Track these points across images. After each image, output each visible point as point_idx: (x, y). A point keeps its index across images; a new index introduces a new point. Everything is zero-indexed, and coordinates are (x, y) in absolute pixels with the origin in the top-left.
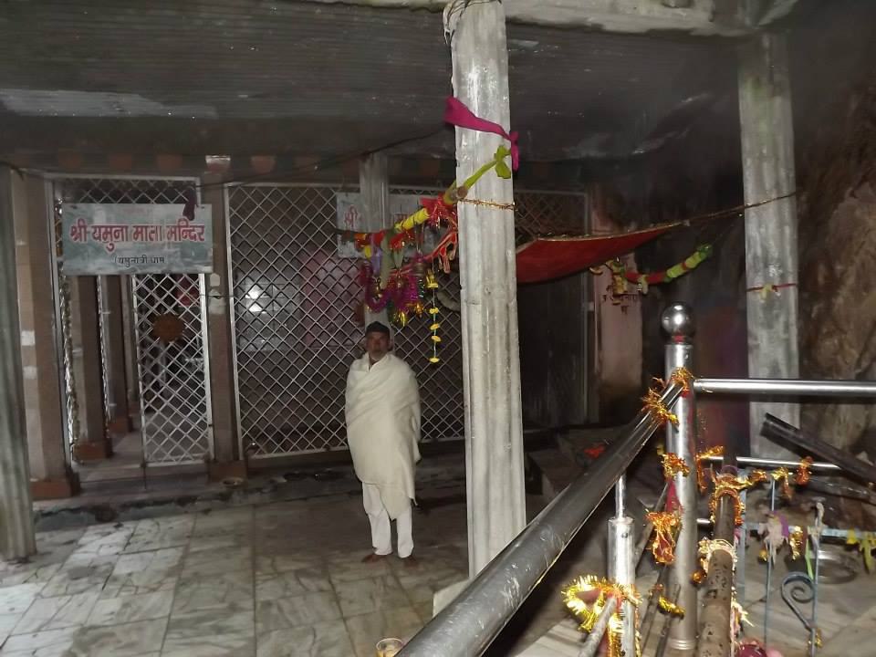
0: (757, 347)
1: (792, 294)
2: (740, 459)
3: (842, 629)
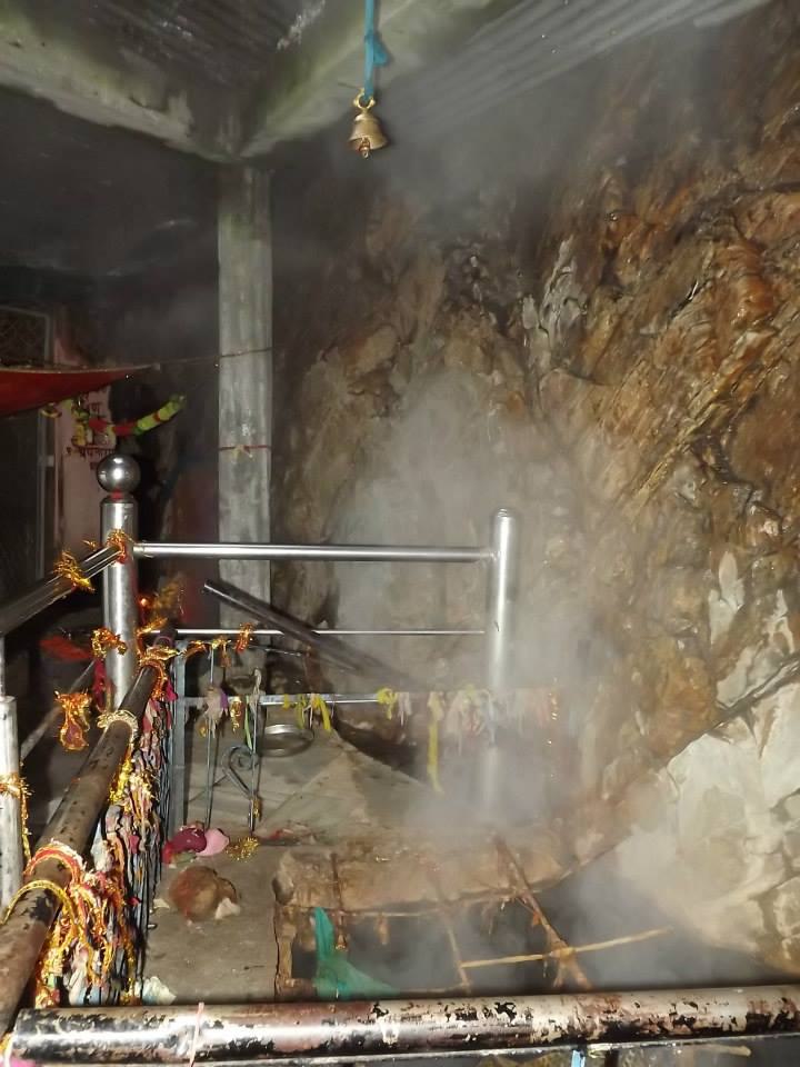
0: (228, 512)
1: (265, 458)
2: (180, 631)
3: (290, 798)
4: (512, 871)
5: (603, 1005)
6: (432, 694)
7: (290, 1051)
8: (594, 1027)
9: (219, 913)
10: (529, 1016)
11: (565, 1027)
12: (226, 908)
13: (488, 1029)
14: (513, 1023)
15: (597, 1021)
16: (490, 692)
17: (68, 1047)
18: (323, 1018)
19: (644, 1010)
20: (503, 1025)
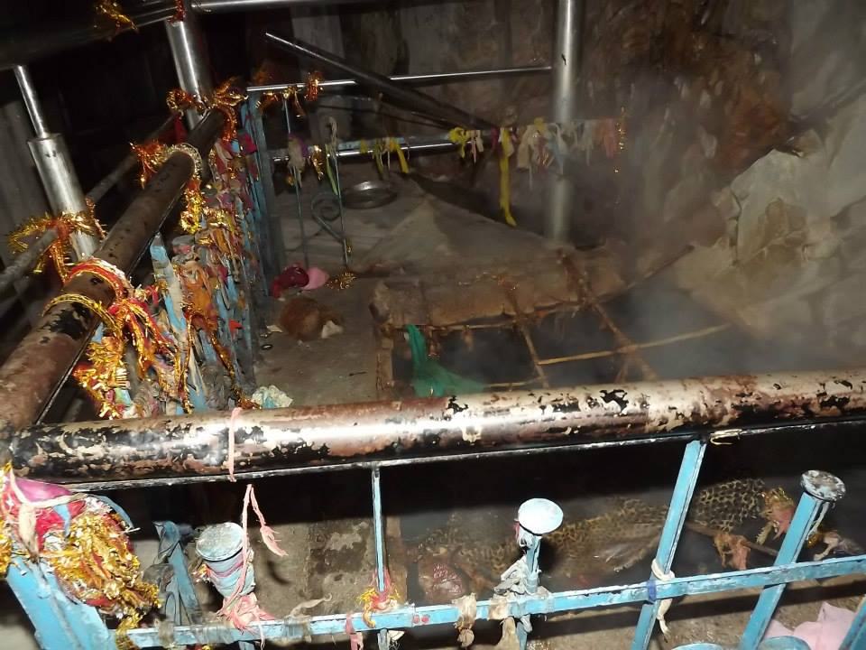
3: (381, 240)
4: (581, 286)
5: (735, 387)
6: (502, 130)
7: (348, 455)
8: (725, 412)
9: (325, 333)
10: (644, 403)
11: (688, 414)
12: (329, 329)
13: (593, 420)
14: (624, 412)
15: (728, 406)
16: (559, 125)
17: (78, 464)
18: (386, 417)
19: (786, 392)
20: (612, 415)
